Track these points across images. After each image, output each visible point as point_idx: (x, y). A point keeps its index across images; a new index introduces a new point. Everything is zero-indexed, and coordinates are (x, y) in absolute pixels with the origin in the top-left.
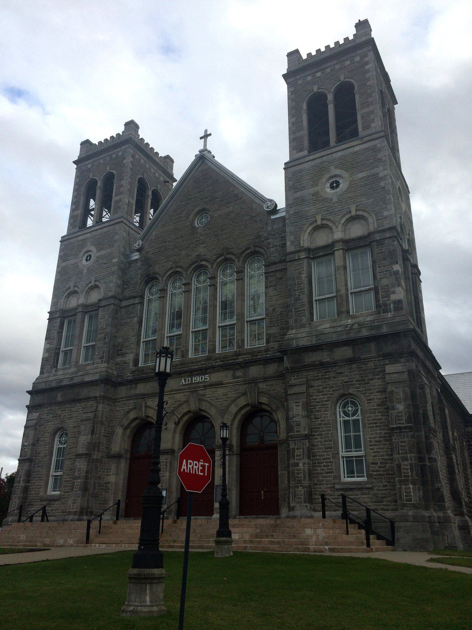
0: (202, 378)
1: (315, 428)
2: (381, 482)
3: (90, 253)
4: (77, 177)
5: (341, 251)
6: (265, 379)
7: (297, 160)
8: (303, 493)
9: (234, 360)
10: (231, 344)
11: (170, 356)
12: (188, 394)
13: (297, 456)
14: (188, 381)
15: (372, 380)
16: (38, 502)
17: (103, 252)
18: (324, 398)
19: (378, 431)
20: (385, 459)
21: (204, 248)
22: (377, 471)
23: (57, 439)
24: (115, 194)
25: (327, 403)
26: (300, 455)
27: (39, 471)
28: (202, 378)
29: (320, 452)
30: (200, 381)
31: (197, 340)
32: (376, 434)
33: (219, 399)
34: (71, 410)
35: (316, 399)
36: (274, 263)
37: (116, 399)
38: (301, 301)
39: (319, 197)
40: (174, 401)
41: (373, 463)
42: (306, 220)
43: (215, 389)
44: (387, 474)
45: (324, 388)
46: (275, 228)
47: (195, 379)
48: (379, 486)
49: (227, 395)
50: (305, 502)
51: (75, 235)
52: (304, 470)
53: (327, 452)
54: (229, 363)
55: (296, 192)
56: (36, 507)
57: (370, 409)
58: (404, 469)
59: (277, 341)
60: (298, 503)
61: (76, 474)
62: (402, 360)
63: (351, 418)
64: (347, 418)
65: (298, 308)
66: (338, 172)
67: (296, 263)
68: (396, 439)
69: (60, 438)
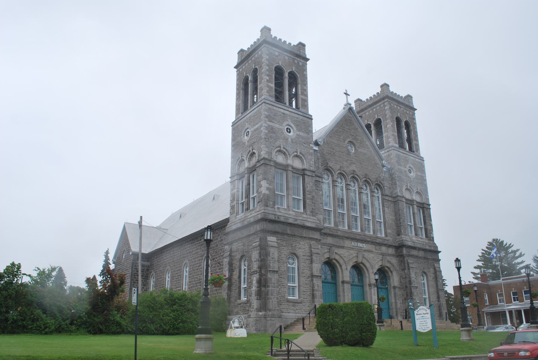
11: (212, 231)
16: (285, 303)
23: (243, 263)
27: (282, 281)
40: (350, 254)
49: (374, 258)
51: (240, 118)
56: (284, 306)
69: (244, 262)
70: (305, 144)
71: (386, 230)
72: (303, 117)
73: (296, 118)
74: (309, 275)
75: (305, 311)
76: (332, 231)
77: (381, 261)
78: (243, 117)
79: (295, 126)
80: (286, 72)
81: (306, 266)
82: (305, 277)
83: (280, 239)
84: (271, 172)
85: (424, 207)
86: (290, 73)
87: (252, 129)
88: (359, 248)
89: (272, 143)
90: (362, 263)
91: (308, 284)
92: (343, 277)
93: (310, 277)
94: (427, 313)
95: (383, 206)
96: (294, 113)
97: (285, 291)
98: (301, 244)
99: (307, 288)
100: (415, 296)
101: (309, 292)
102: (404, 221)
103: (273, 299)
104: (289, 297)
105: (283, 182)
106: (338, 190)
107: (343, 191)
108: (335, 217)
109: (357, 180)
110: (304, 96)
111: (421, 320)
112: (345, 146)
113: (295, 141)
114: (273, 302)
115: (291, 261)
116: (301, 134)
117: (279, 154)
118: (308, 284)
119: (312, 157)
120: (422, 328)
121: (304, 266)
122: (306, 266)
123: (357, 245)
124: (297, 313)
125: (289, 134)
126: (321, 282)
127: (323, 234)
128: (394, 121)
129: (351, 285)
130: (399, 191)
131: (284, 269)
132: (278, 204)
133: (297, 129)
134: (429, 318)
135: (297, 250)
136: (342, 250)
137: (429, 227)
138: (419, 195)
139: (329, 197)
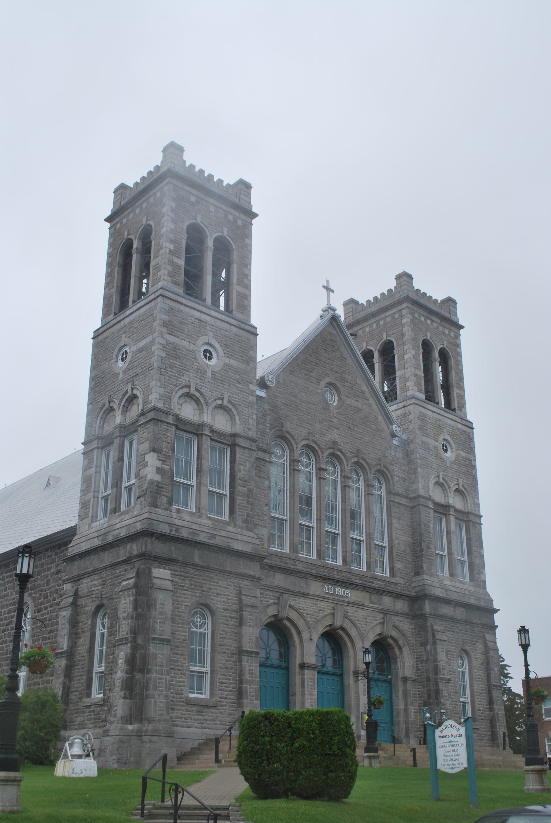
3: (211, 350)
16: (182, 706)
19: (481, 685)
20: (485, 708)
24: (398, 359)
27: (177, 662)
34: (218, 583)
36: (398, 495)
43: (356, 609)
49: (366, 619)
55: (424, 435)
65: (430, 556)
69: (103, 619)
70: (239, 383)
71: (393, 562)
72: (238, 330)
73: (223, 330)
77: (381, 625)
78: (117, 323)
80: (209, 238)
82: (225, 653)
83: (178, 575)
84: (168, 436)
85: (469, 521)
86: (217, 240)
87: (134, 348)
90: (342, 628)
91: (231, 668)
92: (302, 656)
93: (235, 654)
94: (460, 735)
95: (389, 515)
97: (184, 682)
101: (231, 686)
102: (428, 547)
104: (191, 695)
105: (191, 458)
106: (302, 479)
107: (310, 481)
108: (294, 535)
111: (448, 749)
112: (320, 391)
114: (158, 704)
115: (199, 620)
116: (232, 362)
118: (231, 668)
120: (448, 765)
121: (224, 631)
123: (335, 592)
124: (205, 728)
125: (210, 363)
126: (258, 665)
128: (419, 347)
129: (318, 673)
130: (423, 486)
132: (178, 503)
133: (225, 353)
134: (462, 745)
135: (212, 597)
136: (303, 600)
137: (477, 561)
139: (281, 493)
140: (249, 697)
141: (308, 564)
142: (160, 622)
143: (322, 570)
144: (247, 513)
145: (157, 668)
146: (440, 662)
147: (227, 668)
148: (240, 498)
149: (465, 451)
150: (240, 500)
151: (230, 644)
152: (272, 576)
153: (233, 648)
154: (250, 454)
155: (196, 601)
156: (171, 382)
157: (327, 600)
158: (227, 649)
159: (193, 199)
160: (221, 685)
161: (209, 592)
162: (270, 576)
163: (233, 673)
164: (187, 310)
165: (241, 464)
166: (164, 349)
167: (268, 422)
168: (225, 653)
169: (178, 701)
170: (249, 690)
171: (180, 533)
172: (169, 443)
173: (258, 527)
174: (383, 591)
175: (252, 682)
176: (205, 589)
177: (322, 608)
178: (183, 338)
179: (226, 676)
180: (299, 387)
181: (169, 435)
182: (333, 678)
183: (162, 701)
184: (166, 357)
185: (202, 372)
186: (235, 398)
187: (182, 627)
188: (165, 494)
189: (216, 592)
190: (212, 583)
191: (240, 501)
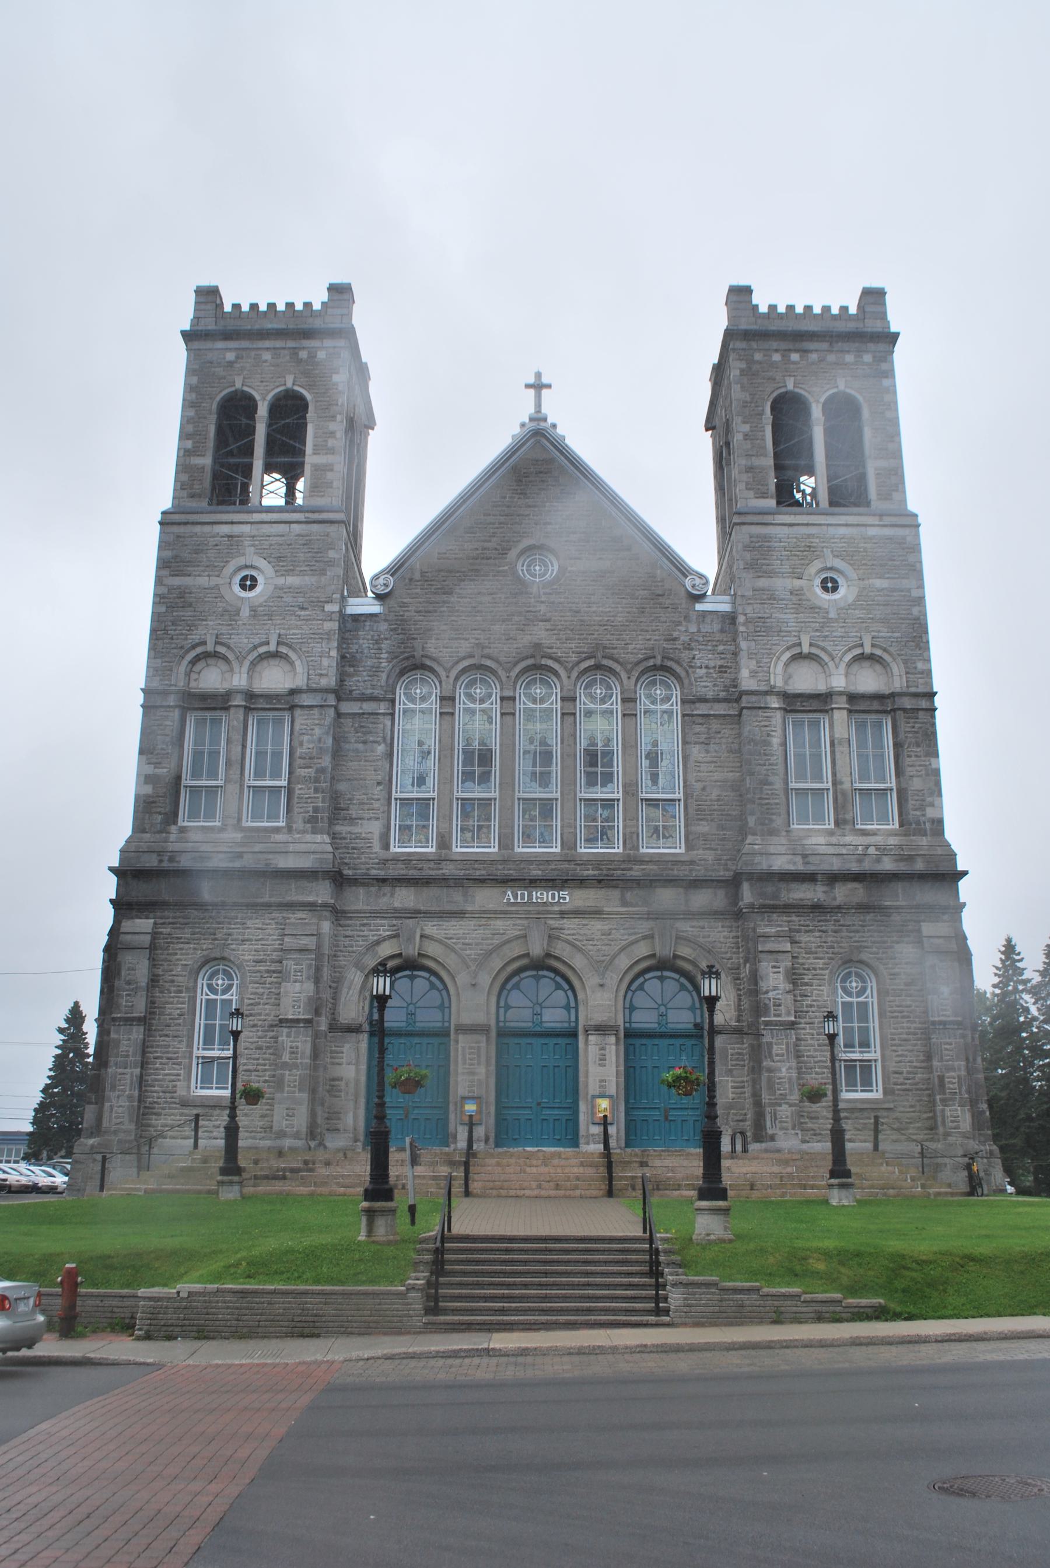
0: (553, 895)
1: (801, 1012)
2: (908, 1101)
3: (254, 573)
4: (190, 372)
5: (845, 712)
6: (690, 915)
7: (759, 514)
8: (789, 1114)
9: (623, 870)
10: (605, 837)
12: (525, 922)
13: (777, 1055)
14: (523, 898)
15: (898, 943)
16: (176, 1109)
17: (291, 580)
18: (818, 963)
20: (915, 1067)
21: (547, 630)
22: (901, 1084)
25: (823, 972)
26: (783, 1055)
28: (553, 895)
29: (809, 1051)
30: (550, 900)
31: (527, 816)
32: (903, 1028)
33: (592, 940)
35: (803, 964)
36: (704, 700)
37: (344, 912)
38: (771, 787)
39: (804, 600)
41: (896, 1073)
42: (778, 636)
43: (585, 922)
44: (917, 1089)
45: (819, 947)
46: (703, 630)
47: (539, 895)
48: (904, 1107)
50: (793, 1128)
52: (790, 1079)
53: (822, 1051)
54: (612, 875)
55: (759, 577)
56: (169, 1118)
57: (893, 989)
58: (950, 1082)
59: (711, 849)
60: (782, 1129)
61: (286, 1058)
62: (946, 917)
63: (219, 997)
64: (213, 997)
66: (838, 563)
67: (760, 712)
68: (937, 1039)
70: (303, 608)
72: (303, 526)
73: (274, 536)
74: (273, 1020)
75: (247, 1131)
76: (415, 868)
79: (269, 563)
81: (267, 991)
82: (255, 1026)
83: (170, 924)
84: (167, 725)
88: (537, 909)
89: (177, 639)
91: (268, 1048)
96: (270, 522)
97: (178, 1075)
98: (248, 928)
99: (260, 1061)
100: (776, 1058)
101: (268, 1073)
103: (114, 1102)
109: (493, 672)
110: (327, 454)
112: (506, 568)
113: (264, 610)
114: (115, 1109)
117: (208, 665)
118: (268, 1048)
119: (328, 643)
121: (256, 993)
122: (267, 991)
124: (217, 1139)
127: (375, 882)
131: (178, 1009)
133: (276, 571)
135: (233, 946)
136: (455, 923)
138: (814, 662)
140: (286, 1089)
141: (469, 863)
142: (128, 995)
143: (500, 867)
144: (313, 807)
145: (119, 1059)
146: (767, 992)
147: (260, 1048)
148: (300, 786)
149: (887, 576)
150: (300, 789)
151: (267, 1012)
152: (389, 895)
153: (272, 1017)
154: (321, 714)
155: (203, 956)
156: (173, 646)
157: (508, 916)
158: (260, 1020)
159: (230, 356)
160: (248, 1073)
161: (226, 940)
162: (384, 895)
163: (270, 1054)
164: (207, 529)
165: (304, 734)
166: (162, 601)
167: (384, 651)
168: (255, 1026)
169: (166, 1102)
170: (287, 1078)
171: (177, 862)
172: (167, 735)
173: (360, 821)
174: (651, 880)
175: (295, 1066)
176: (219, 936)
177: (499, 930)
178: (198, 573)
179: (258, 1059)
180: (457, 575)
181: (169, 723)
182: (560, 1040)
183: (123, 1104)
184: (167, 611)
185: (232, 614)
186: (294, 634)
187: (177, 997)
188: (159, 810)
189: (241, 937)
190: (233, 926)
191: (300, 792)
